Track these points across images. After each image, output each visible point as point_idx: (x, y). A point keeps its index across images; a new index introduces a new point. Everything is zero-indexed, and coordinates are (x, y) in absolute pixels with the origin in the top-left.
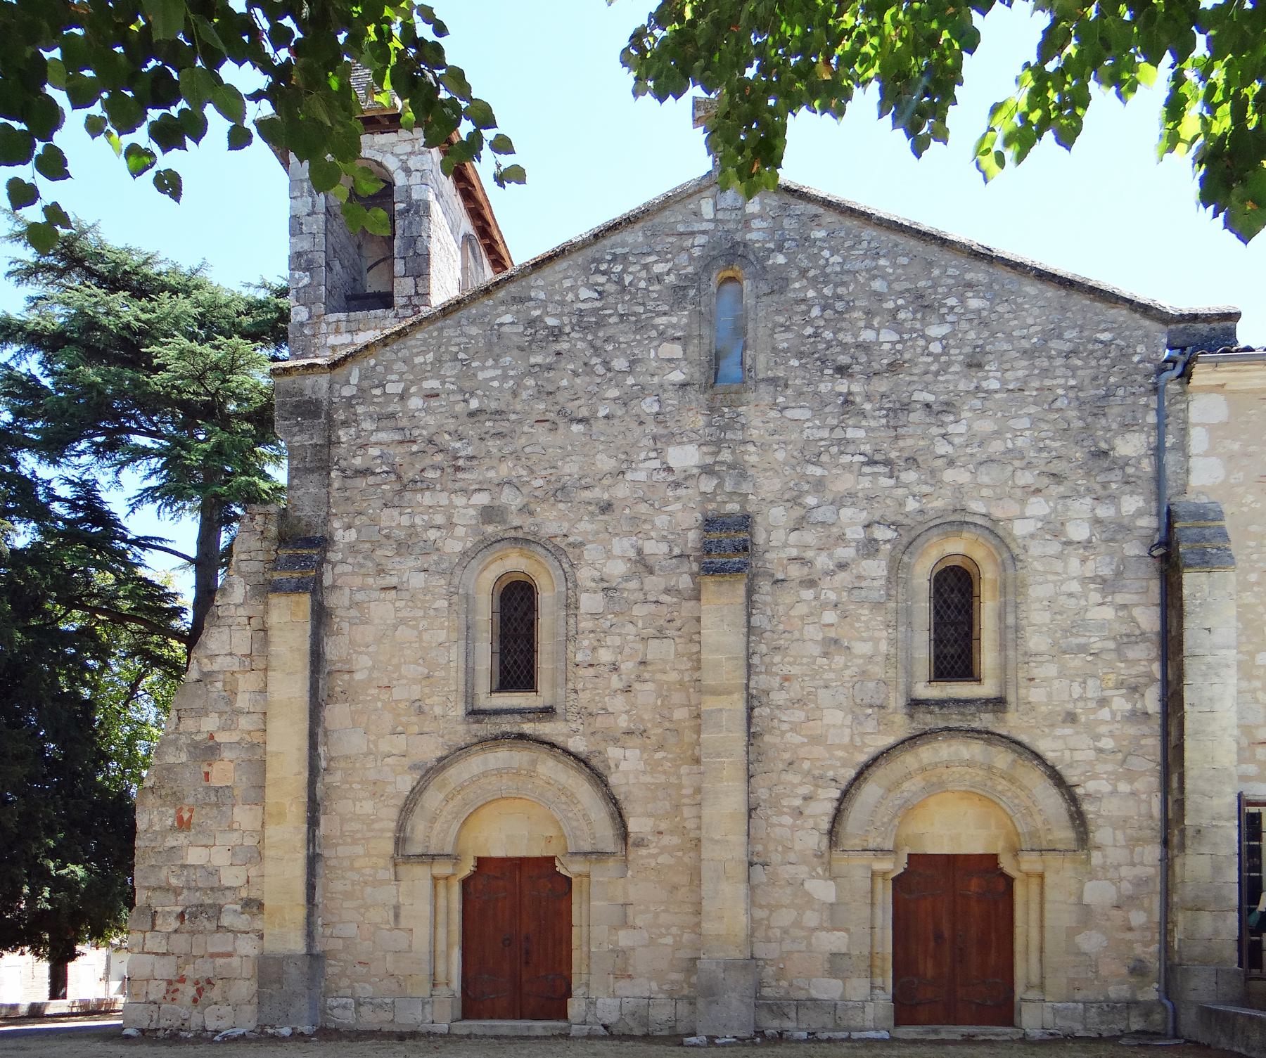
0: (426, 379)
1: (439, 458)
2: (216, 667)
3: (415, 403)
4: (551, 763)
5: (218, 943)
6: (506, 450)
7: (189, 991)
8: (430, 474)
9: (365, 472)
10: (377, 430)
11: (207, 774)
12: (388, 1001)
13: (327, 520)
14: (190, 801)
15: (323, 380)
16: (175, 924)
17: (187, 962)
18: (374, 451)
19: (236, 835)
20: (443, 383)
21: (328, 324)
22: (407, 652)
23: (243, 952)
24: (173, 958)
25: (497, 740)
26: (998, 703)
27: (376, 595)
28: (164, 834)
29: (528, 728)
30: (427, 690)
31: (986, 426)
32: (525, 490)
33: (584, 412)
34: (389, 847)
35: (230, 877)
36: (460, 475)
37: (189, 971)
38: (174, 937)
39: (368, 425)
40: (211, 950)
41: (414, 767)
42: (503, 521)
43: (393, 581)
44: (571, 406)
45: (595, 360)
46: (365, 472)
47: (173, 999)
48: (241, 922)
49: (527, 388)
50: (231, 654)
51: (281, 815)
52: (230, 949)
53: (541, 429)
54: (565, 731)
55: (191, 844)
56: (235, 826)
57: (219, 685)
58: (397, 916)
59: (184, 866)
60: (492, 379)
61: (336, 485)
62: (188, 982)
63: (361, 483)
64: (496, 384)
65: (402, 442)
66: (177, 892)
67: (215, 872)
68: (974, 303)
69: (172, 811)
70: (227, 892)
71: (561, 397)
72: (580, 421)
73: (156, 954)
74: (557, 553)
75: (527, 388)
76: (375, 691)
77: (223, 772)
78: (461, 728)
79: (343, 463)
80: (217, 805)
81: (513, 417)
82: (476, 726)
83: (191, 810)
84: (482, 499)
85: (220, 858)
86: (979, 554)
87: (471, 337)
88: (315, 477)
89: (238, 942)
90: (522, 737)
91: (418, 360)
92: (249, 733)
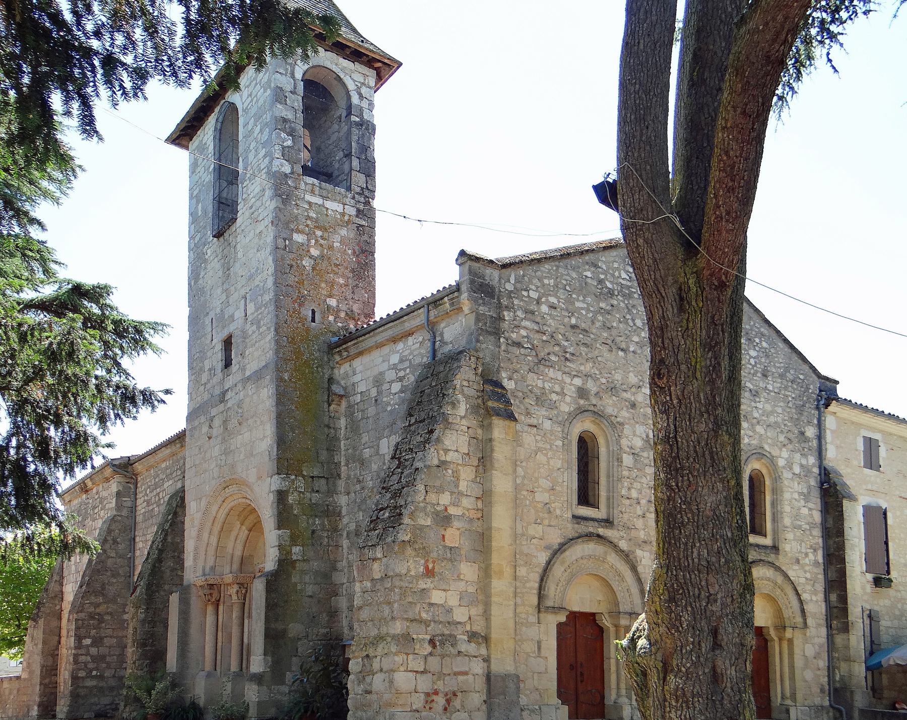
0: (550, 295)
1: (557, 348)
2: (448, 459)
3: (544, 308)
4: (613, 555)
5: (459, 664)
6: (589, 356)
7: (440, 700)
8: (553, 358)
9: (518, 345)
10: (525, 318)
11: (444, 536)
12: (537, 707)
13: (498, 372)
14: (434, 555)
15: (496, 274)
16: (429, 649)
17: (439, 679)
18: (523, 332)
19: (463, 583)
20: (559, 302)
21: (306, 184)
22: (542, 470)
23: (476, 671)
24: (430, 675)
25: (589, 536)
26: (608, 522)
27: (526, 428)
28: (417, 577)
29: (601, 531)
30: (552, 498)
31: (768, 407)
32: (598, 383)
33: (623, 346)
34: (535, 601)
35: (460, 615)
36: (568, 364)
37: (440, 685)
38: (430, 659)
39: (520, 314)
40: (456, 670)
41: (547, 548)
42: (587, 399)
43: (534, 422)
44: (618, 339)
45: (628, 317)
46: (518, 345)
47: (430, 708)
48: (472, 648)
49: (599, 321)
50: (457, 451)
51: (500, 573)
52: (467, 669)
53: (605, 348)
54: (618, 536)
55: (435, 588)
56: (462, 577)
57: (450, 471)
58: (539, 648)
59: (432, 604)
60: (582, 309)
61: (503, 347)
62: (441, 695)
63: (516, 351)
64: (584, 312)
65: (538, 332)
66: (427, 623)
67: (449, 611)
68: (764, 344)
69: (423, 562)
70: (458, 626)
71: (614, 332)
72: (622, 350)
73: (417, 672)
74: (613, 426)
75: (599, 321)
76: (525, 493)
77: (453, 536)
78: (570, 526)
79: (507, 334)
80: (450, 560)
81: (592, 336)
82: (576, 526)
83: (434, 562)
84: (578, 382)
85: (453, 601)
86: (764, 471)
87: (573, 279)
88: (492, 338)
89: (472, 664)
90: (599, 536)
91: (546, 281)
92: (468, 510)
